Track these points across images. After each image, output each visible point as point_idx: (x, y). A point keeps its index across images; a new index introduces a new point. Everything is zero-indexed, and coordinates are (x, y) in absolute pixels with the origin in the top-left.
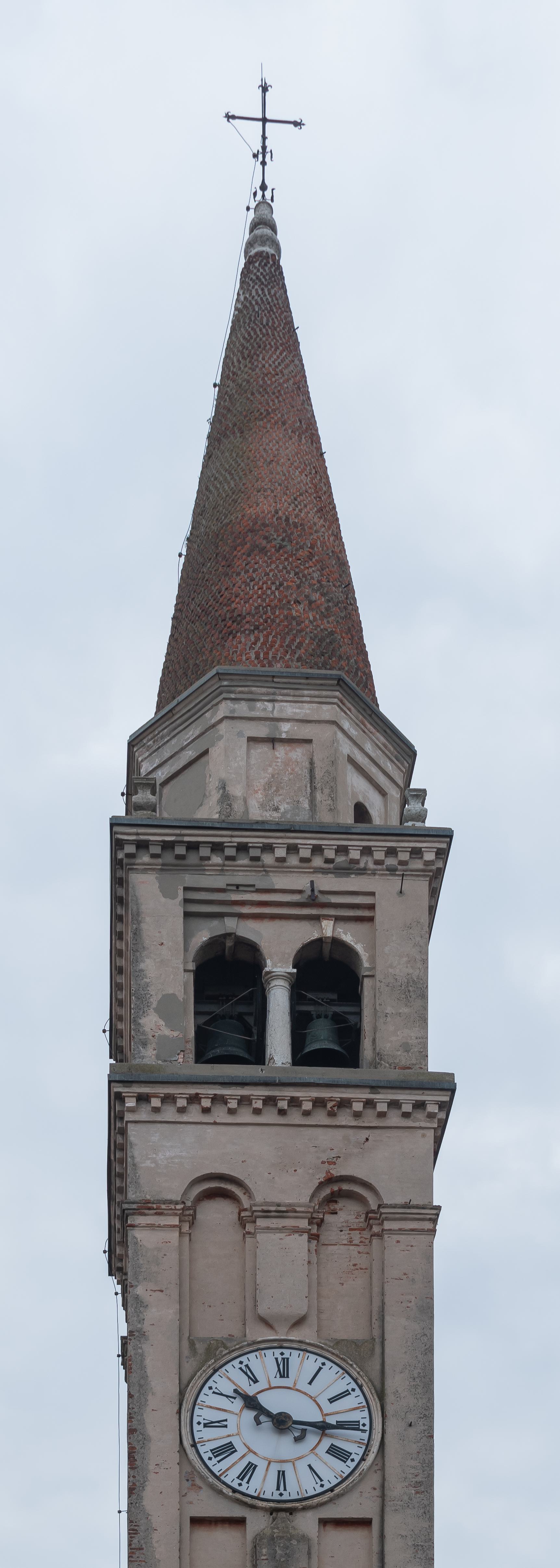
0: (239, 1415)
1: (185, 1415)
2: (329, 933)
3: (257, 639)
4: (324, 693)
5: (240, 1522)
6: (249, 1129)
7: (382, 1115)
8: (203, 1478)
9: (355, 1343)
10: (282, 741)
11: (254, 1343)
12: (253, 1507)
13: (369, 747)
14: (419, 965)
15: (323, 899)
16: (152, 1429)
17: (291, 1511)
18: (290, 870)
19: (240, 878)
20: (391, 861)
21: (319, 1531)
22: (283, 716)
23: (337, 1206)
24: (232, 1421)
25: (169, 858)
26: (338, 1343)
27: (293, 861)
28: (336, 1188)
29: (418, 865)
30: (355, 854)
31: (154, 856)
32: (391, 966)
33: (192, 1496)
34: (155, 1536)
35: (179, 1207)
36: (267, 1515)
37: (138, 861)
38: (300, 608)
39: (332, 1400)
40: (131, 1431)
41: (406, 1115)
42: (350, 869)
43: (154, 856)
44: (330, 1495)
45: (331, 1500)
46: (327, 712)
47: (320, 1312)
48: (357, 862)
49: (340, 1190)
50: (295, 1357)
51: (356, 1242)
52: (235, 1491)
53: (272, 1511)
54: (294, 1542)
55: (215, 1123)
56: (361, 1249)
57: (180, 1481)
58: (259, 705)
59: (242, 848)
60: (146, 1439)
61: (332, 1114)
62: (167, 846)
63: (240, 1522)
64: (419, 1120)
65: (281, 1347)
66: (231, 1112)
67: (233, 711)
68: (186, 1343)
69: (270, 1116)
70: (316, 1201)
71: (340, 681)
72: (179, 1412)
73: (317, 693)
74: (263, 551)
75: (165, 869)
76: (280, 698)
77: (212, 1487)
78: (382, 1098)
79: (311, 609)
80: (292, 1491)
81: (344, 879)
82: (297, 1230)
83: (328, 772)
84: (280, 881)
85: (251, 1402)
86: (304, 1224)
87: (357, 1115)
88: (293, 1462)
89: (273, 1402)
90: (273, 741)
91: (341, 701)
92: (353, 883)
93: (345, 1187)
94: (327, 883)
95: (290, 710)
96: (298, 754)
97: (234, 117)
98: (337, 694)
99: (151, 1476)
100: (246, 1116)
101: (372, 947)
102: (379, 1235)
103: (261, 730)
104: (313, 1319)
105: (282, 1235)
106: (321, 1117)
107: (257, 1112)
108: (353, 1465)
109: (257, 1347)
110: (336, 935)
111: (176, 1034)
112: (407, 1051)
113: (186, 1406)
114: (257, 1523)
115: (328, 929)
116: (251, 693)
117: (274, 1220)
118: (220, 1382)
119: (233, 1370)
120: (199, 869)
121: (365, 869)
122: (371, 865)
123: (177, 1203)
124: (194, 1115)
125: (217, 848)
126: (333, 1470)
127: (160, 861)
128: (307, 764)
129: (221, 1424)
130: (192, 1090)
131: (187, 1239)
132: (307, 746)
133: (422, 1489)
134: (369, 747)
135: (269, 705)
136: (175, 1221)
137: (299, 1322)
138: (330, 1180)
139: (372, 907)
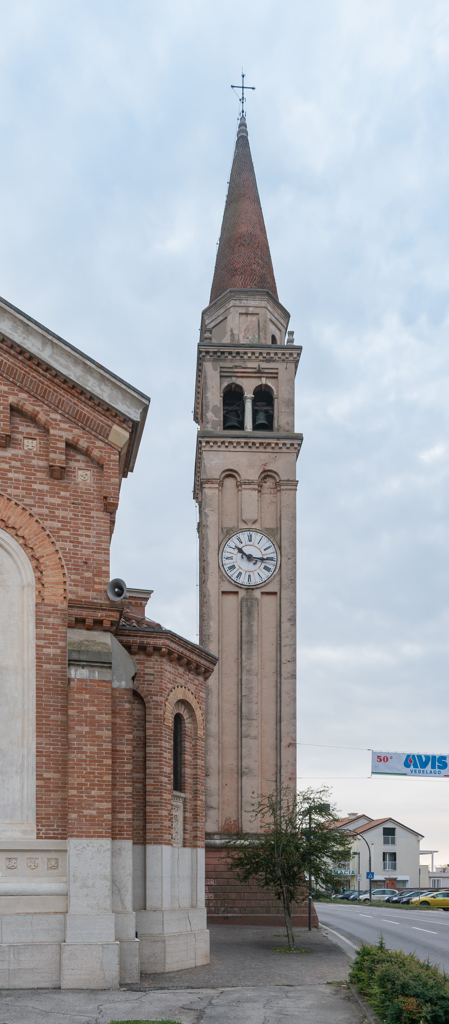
1: (220, 555)
4: (263, 297)
5: (236, 593)
7: (280, 448)
8: (226, 577)
10: (250, 314)
12: (241, 588)
13: (276, 315)
15: (262, 371)
17: (252, 589)
19: (237, 364)
20: (283, 357)
23: (266, 480)
25: (215, 357)
26: (267, 529)
28: (266, 474)
29: (291, 358)
31: (211, 356)
32: (283, 395)
33: (222, 584)
34: (211, 598)
35: (218, 481)
36: (245, 591)
38: (255, 266)
39: (265, 550)
41: (288, 448)
43: (211, 356)
44: (264, 583)
46: (264, 303)
48: (273, 358)
50: (253, 534)
52: (235, 582)
53: (247, 589)
54: (253, 600)
55: (229, 451)
58: (243, 301)
59: (238, 353)
61: (265, 448)
62: (215, 353)
63: (236, 593)
65: (249, 531)
66: (234, 447)
67: (235, 304)
69: (246, 449)
70: (260, 479)
71: (268, 293)
72: (218, 554)
74: (244, 245)
75: (214, 360)
76: (249, 299)
77: (228, 580)
78: (281, 442)
80: (253, 582)
82: (254, 489)
83: (264, 325)
84: (249, 365)
85: (240, 551)
86: (256, 487)
87: (273, 448)
88: (253, 572)
89: (247, 550)
90: (247, 314)
93: (269, 473)
94: (264, 365)
95: (252, 303)
96: (255, 318)
97: (234, 87)
98: (267, 297)
99: (210, 577)
100: (239, 449)
103: (243, 310)
105: (250, 491)
106: (262, 449)
107: (242, 447)
108: (271, 573)
109: (242, 531)
111: (217, 419)
113: (221, 551)
114: (242, 593)
115: (264, 381)
117: (247, 486)
119: (234, 539)
120: (225, 360)
121: (275, 360)
122: (277, 359)
124: (223, 448)
125: (230, 353)
127: (212, 358)
129: (231, 558)
130: (222, 440)
133: (293, 582)
134: (276, 315)
135: (246, 302)
136: (217, 486)
137: (255, 522)
138: (265, 471)
139: (277, 373)
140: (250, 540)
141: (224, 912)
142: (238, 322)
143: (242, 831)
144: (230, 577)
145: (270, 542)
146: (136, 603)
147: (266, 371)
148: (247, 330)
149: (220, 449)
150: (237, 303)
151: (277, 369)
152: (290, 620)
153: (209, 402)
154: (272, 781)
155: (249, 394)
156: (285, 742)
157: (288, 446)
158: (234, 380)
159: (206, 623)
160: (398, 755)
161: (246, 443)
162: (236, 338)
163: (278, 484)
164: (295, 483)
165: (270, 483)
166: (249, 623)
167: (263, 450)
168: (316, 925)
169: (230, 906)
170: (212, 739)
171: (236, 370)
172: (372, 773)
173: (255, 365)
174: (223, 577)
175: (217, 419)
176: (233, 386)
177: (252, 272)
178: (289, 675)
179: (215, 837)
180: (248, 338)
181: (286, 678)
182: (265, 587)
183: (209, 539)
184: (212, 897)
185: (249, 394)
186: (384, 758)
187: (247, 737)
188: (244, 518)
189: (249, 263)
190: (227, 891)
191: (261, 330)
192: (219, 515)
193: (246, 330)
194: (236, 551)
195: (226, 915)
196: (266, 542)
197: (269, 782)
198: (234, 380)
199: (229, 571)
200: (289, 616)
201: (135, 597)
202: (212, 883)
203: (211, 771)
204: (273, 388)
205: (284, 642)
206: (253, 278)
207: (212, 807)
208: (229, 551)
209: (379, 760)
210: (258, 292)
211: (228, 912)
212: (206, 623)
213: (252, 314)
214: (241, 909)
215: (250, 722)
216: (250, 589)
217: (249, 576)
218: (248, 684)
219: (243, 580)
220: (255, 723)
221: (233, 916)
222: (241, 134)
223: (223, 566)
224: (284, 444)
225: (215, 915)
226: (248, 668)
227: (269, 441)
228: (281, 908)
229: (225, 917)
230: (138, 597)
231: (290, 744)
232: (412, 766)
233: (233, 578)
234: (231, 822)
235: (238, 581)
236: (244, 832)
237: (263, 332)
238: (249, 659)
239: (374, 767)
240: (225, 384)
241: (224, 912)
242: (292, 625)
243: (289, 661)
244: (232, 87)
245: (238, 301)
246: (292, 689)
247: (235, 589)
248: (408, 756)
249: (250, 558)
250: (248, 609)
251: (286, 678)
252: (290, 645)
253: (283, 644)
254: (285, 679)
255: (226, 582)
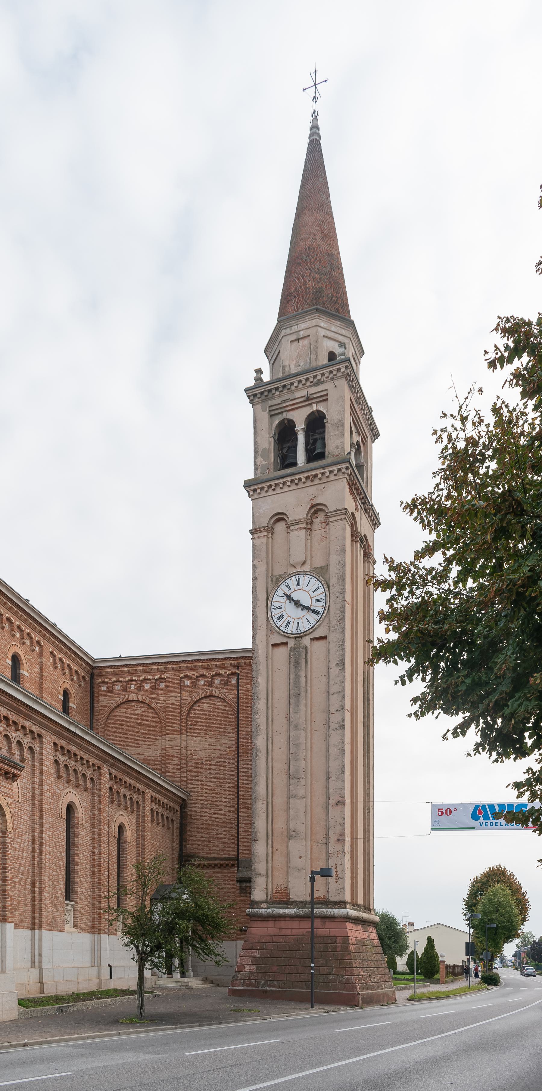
0: (285, 603)
1: (269, 606)
2: (315, 409)
3: (295, 301)
4: (313, 316)
5: (285, 644)
6: (288, 493)
7: (328, 477)
8: (275, 629)
9: (321, 568)
10: (301, 338)
11: (290, 574)
12: (289, 637)
13: (333, 328)
14: (342, 413)
15: (311, 397)
16: (258, 614)
17: (301, 637)
18: (301, 389)
19: (285, 397)
20: (331, 376)
21: (311, 643)
22: (301, 329)
23: (317, 515)
24: (283, 605)
25: (263, 397)
26: (316, 569)
27: (301, 386)
28: (315, 509)
29: (340, 374)
30: (319, 377)
31: (259, 398)
32: (332, 417)
33: (272, 636)
34: (259, 654)
35: (266, 528)
36: (294, 640)
37: (254, 401)
38: (310, 283)
39: (313, 592)
40: (253, 615)
41: (336, 475)
42: (319, 383)
43: (259, 398)
44: (313, 628)
45: (313, 631)
46: (314, 322)
47: (311, 557)
48: (320, 380)
49: (317, 509)
50: (302, 577)
51: (323, 527)
52: (284, 632)
53: (296, 638)
54: (301, 649)
55: (277, 494)
56: (325, 530)
57: (267, 631)
58: (293, 328)
59: (284, 386)
60: (257, 617)
61: (312, 481)
62: (262, 393)
63: (285, 644)
64: (340, 476)
65: (298, 574)
66: (281, 488)
67: (285, 333)
68: (270, 579)
69: (294, 487)
70: (309, 515)
71: (317, 310)
72: (267, 606)
73: (310, 316)
74: (300, 264)
75: (263, 401)
76: (299, 323)
77: (277, 632)
78: (327, 470)
79: (314, 281)
80: (302, 629)
81: (318, 387)
82: (302, 529)
83: (315, 346)
84: (298, 394)
85: (289, 597)
86: (304, 525)
87: (320, 479)
88: (301, 618)
89: (295, 596)
90: (298, 340)
91: (319, 316)
92: (321, 388)
93: (318, 507)
94: (312, 390)
95: (303, 326)
96: (306, 342)
97: (306, 89)
98: (317, 314)
99: (258, 631)
100: (286, 489)
101: (327, 411)
102: (328, 524)
103: (294, 337)
104: (308, 562)
105: (297, 532)
106: (309, 483)
107: (289, 486)
108: (320, 616)
109: (291, 576)
110: (317, 409)
111: (266, 463)
112: (338, 449)
113: (269, 603)
114: (291, 643)
115: (314, 407)
116: (290, 324)
117: (295, 526)
118: (280, 592)
119: (283, 587)
120: (273, 398)
121: (323, 381)
122: (325, 379)
123: (265, 527)
124: (271, 492)
125: (277, 389)
126: (314, 619)
127: (261, 399)
128: (309, 345)
129: (280, 607)
130: (268, 484)
131: (270, 539)
132: (309, 337)
133: (341, 622)
134: (333, 328)
135: (296, 327)
136: (265, 533)
137: (304, 563)
138: (313, 506)
139: (327, 395)
140: (299, 585)
141: (264, 985)
142: (288, 352)
143: (289, 898)
144: (279, 628)
145: (319, 582)
146: (245, 663)
147: (315, 396)
148: (299, 357)
149: (268, 494)
150: (288, 331)
151: (327, 390)
152: (338, 664)
153: (258, 446)
154: (323, 843)
155: (300, 426)
156: (333, 801)
157: (335, 472)
158: (285, 415)
159: (255, 681)
160: (464, 806)
161: (292, 481)
162: (287, 369)
163: (327, 517)
164: (253, 532)
165: (321, 517)
166: (296, 675)
167: (311, 484)
168: (356, 1004)
169: (270, 979)
170: (261, 802)
171: (285, 405)
172: (432, 829)
173: (303, 393)
174: (272, 629)
175: (266, 463)
176: (286, 422)
177: (306, 290)
178: (337, 725)
179: (263, 906)
180: (299, 365)
181: (335, 729)
182: (314, 632)
183: (258, 592)
184: (254, 969)
185: (300, 426)
186: (446, 810)
187: (294, 797)
188: (292, 562)
189: (303, 282)
190: (269, 964)
191: (312, 352)
192: (267, 564)
193: (297, 357)
194: (285, 598)
195: (265, 989)
196: (315, 583)
197: (319, 845)
198: (285, 415)
199: (278, 621)
200: (337, 660)
201: (243, 657)
202: (256, 954)
203: (260, 835)
204: (325, 411)
205: (334, 689)
206: (307, 297)
207: (260, 874)
208: (278, 599)
209: (440, 813)
210: (306, 312)
211: (270, 986)
212: (255, 681)
213: (303, 338)
214: (281, 983)
215: (297, 781)
216: (299, 637)
217: (298, 623)
218: (295, 741)
219: (292, 629)
220: (302, 782)
221: (271, 990)
222: (314, 137)
223: (272, 617)
224: (331, 472)
225: (254, 988)
226: (295, 723)
227: (315, 473)
228: (320, 983)
229: (264, 990)
230: (246, 657)
231: (338, 802)
232: (482, 818)
233: (281, 628)
234: (281, 889)
235: (286, 631)
236: (291, 900)
237: (314, 353)
238: (297, 713)
239: (434, 821)
240: (276, 422)
241: (264, 985)
242: (340, 670)
243: (337, 711)
244: (304, 90)
245: (288, 329)
246: (341, 741)
247: (284, 640)
248: (477, 806)
249: (297, 603)
250: (295, 660)
251: (335, 729)
252: (339, 692)
253: (331, 692)
254: (333, 730)
255: (276, 634)
